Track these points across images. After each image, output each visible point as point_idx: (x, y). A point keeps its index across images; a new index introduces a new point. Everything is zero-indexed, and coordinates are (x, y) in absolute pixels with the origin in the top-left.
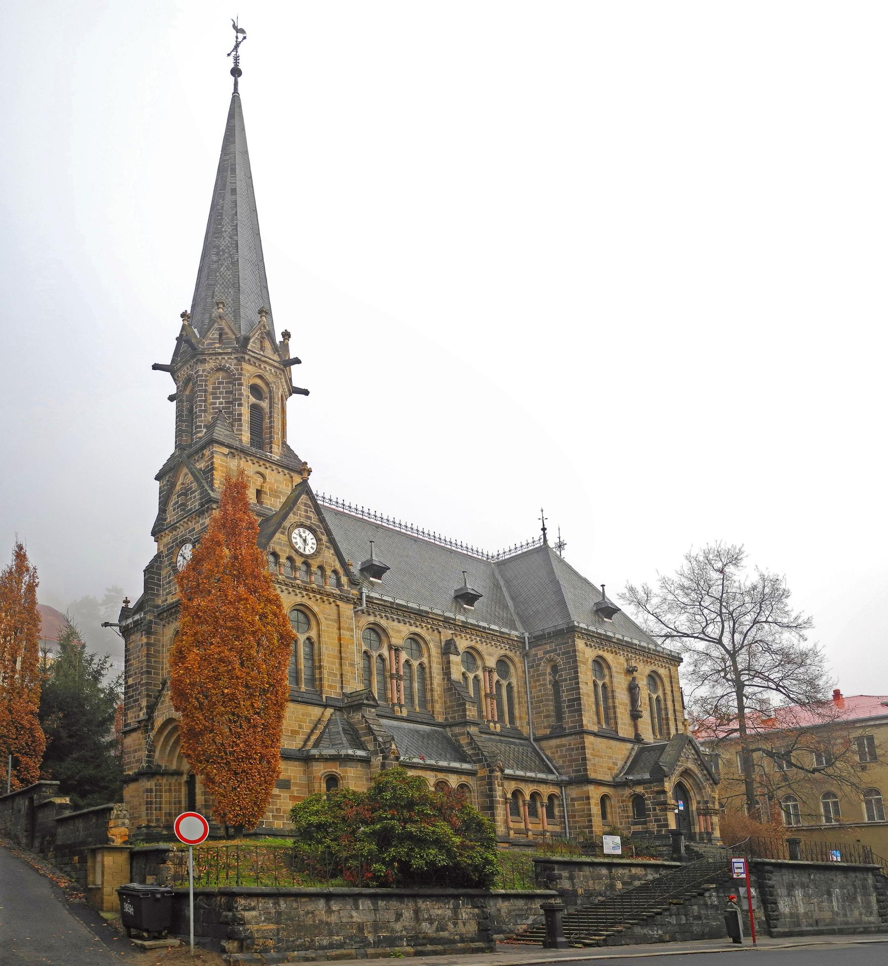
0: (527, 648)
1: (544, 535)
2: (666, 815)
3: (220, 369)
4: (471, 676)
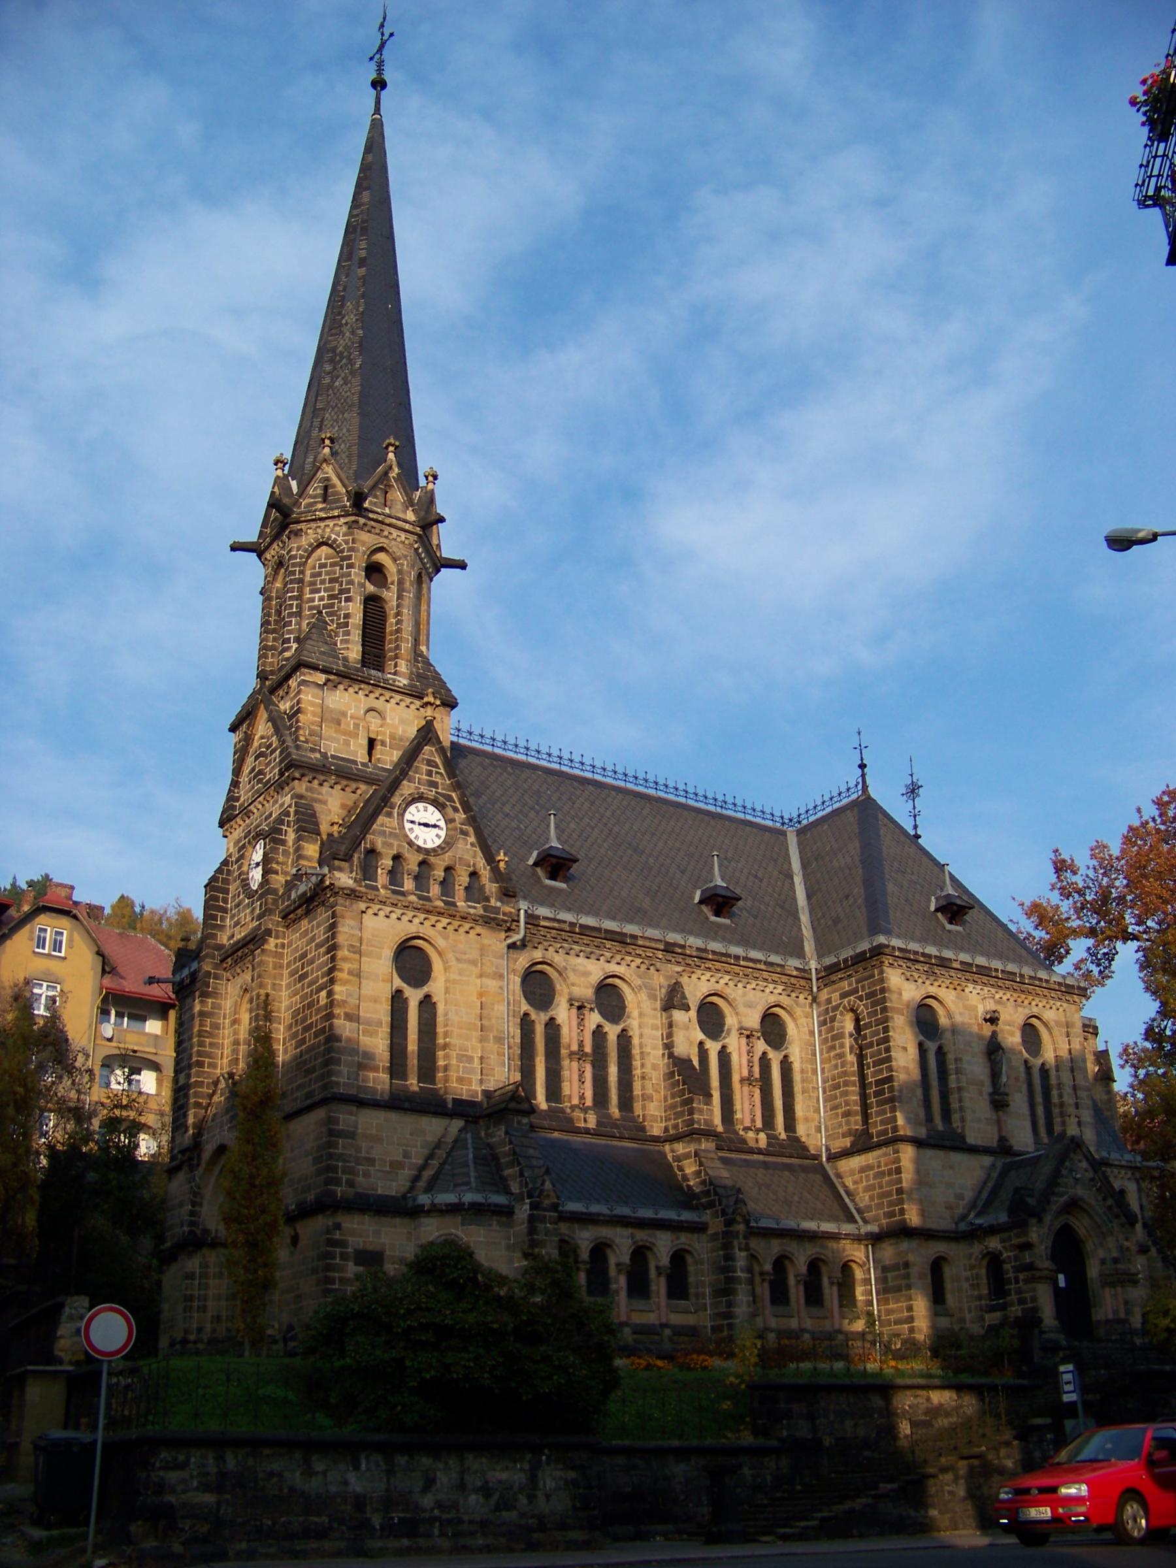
0: (815, 989)
1: (863, 775)
2: (1034, 1290)
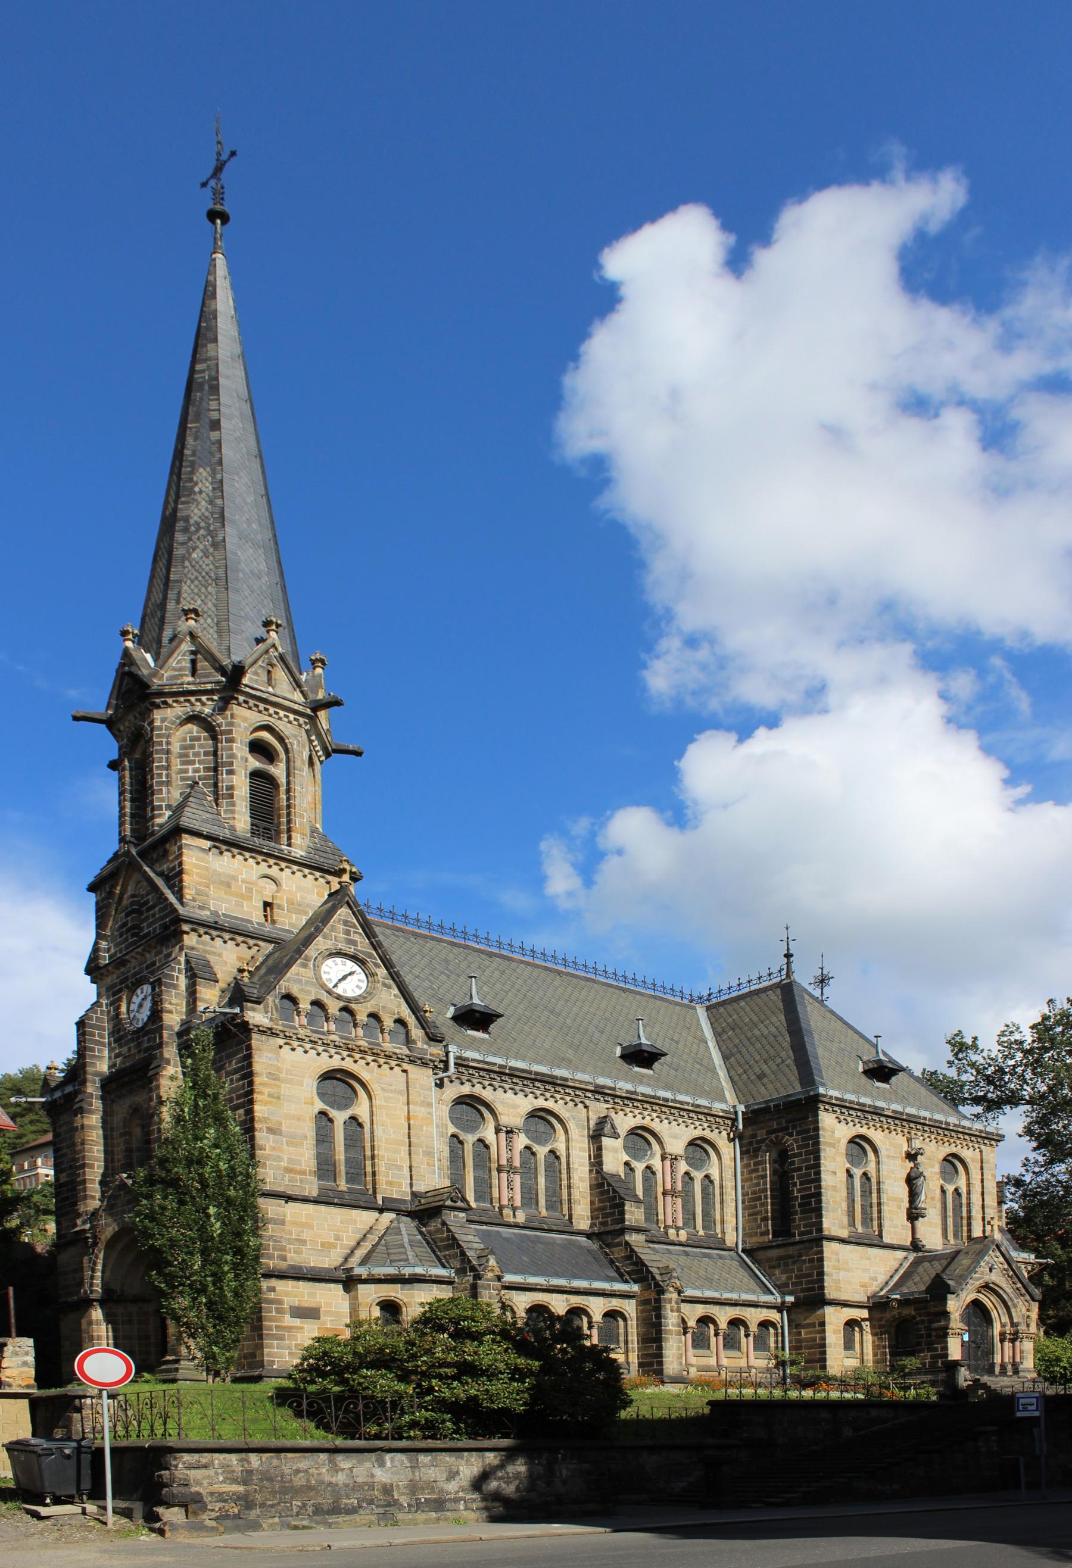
0: (741, 1127)
1: (788, 964)
4: (639, 1167)
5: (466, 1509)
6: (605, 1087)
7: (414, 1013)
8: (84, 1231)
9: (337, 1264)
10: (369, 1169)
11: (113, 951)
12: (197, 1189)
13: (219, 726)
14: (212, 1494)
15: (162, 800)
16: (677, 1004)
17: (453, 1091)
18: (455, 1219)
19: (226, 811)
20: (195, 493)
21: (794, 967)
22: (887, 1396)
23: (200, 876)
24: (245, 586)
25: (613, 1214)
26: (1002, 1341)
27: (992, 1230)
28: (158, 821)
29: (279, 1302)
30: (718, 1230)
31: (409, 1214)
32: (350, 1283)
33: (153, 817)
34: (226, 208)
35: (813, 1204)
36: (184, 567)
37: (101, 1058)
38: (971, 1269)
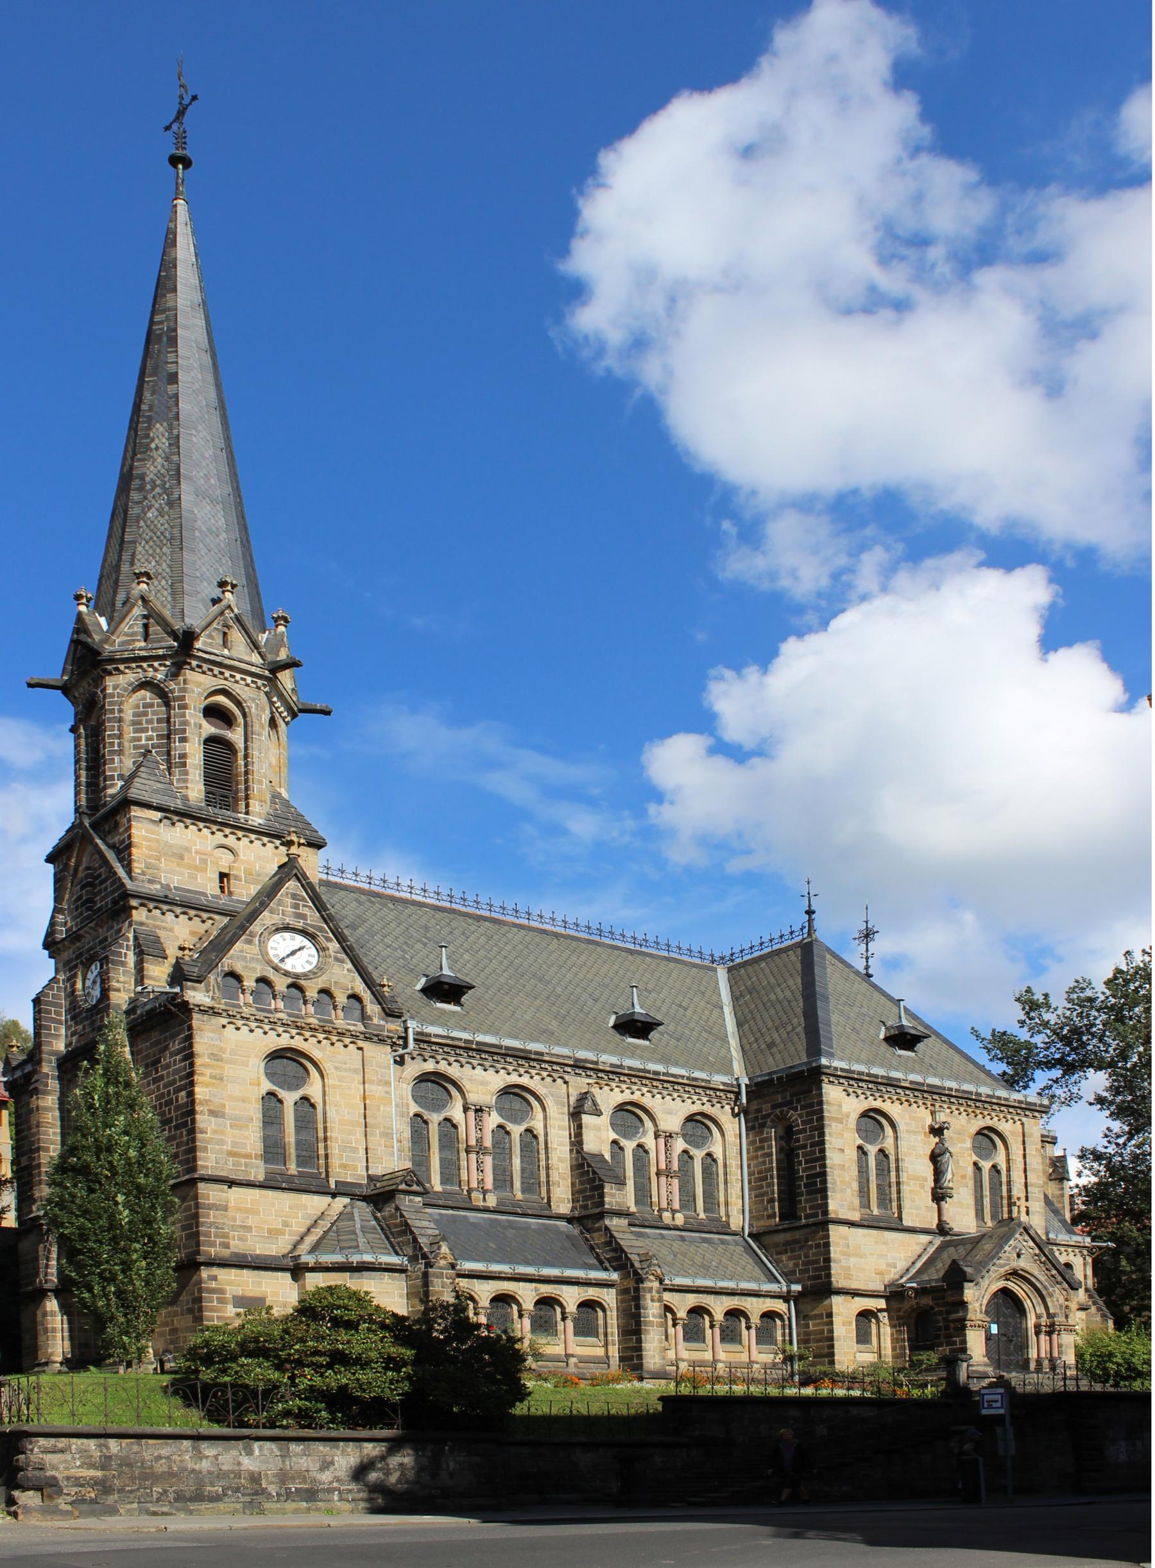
0: (744, 1101)
1: (810, 921)
3: (146, 685)
4: (629, 1145)
5: (340, 1500)
6: (586, 1061)
7: (369, 988)
8: (38, 1217)
9: (285, 1251)
10: (322, 1152)
11: (69, 924)
12: (106, 1177)
13: (172, 692)
14: (68, 1478)
15: (115, 770)
16: (694, 965)
17: (414, 1068)
18: (410, 1204)
19: (178, 780)
20: (151, 450)
21: (816, 924)
22: (901, 1393)
23: (150, 848)
24: (201, 545)
25: (592, 1197)
26: (1037, 1334)
27: (1019, 1212)
28: (110, 791)
29: (221, 1291)
30: (723, 1213)
31: (364, 1198)
32: (297, 1271)
33: (105, 788)
34: (187, 153)
35: (818, 1185)
36: (139, 527)
37: (57, 1036)
38: (993, 1255)
